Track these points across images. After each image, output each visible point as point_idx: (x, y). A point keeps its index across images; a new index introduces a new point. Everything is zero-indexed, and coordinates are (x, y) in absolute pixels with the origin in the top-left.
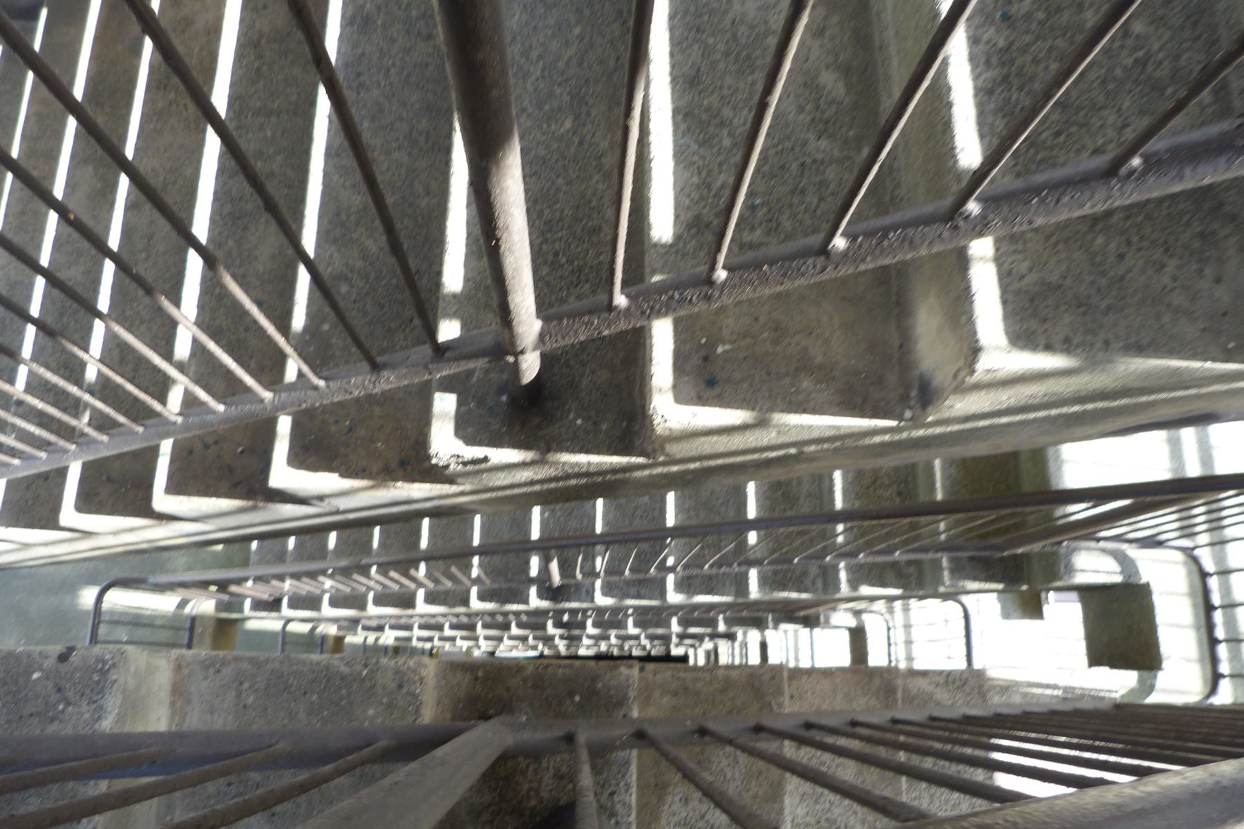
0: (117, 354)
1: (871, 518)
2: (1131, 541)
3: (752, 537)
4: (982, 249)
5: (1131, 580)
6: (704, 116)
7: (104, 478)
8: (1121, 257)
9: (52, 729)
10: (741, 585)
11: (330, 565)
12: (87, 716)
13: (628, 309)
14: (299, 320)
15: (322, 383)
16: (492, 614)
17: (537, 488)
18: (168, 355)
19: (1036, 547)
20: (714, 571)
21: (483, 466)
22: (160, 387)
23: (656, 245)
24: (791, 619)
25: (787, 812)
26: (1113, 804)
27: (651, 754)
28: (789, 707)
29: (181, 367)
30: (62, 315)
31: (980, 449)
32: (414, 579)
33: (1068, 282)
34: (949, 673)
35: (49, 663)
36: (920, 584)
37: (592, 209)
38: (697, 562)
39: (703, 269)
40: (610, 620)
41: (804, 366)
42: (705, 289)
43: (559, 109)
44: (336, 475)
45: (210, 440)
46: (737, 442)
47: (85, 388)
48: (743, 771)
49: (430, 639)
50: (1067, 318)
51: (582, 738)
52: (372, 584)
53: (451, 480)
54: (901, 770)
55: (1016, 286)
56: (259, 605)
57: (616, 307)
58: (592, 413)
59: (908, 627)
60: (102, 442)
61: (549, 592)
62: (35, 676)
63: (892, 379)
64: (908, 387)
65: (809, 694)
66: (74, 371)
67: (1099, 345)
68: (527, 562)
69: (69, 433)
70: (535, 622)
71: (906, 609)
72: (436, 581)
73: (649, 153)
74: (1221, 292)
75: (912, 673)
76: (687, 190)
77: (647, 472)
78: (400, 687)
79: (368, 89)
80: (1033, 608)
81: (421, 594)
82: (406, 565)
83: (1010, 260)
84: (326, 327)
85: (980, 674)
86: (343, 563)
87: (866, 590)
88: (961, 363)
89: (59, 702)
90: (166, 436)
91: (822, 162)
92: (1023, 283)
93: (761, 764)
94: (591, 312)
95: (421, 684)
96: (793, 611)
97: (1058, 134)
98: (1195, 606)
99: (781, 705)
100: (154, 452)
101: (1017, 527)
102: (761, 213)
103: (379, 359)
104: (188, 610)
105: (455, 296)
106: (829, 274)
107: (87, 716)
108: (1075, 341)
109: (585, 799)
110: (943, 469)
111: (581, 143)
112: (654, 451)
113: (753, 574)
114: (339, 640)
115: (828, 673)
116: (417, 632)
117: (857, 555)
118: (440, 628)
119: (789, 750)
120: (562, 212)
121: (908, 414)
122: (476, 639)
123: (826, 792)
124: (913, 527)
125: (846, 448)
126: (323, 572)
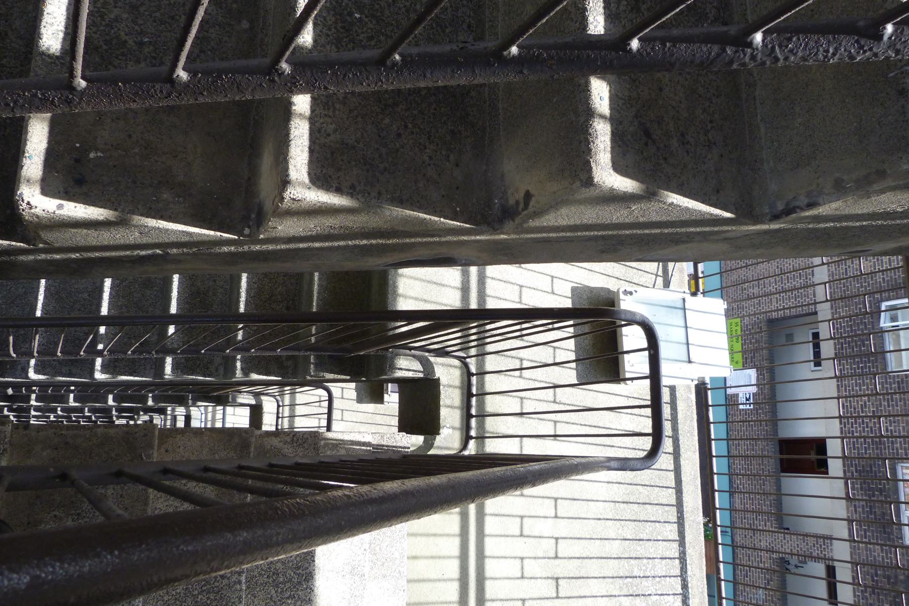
1: (258, 321)
2: (429, 351)
3: (171, 329)
8: (399, 135)
19: (372, 351)
20: (136, 356)
23: (43, 54)
33: (361, 145)
36: (294, 374)
46: (106, 237)
65: (182, 448)
67: (373, 194)
71: (293, 394)
77: (31, 257)
83: (322, 120)
87: (255, 377)
97: (370, 38)
98: (462, 394)
108: (358, 189)
113: (169, 360)
121: (247, 231)
125: (203, 254)
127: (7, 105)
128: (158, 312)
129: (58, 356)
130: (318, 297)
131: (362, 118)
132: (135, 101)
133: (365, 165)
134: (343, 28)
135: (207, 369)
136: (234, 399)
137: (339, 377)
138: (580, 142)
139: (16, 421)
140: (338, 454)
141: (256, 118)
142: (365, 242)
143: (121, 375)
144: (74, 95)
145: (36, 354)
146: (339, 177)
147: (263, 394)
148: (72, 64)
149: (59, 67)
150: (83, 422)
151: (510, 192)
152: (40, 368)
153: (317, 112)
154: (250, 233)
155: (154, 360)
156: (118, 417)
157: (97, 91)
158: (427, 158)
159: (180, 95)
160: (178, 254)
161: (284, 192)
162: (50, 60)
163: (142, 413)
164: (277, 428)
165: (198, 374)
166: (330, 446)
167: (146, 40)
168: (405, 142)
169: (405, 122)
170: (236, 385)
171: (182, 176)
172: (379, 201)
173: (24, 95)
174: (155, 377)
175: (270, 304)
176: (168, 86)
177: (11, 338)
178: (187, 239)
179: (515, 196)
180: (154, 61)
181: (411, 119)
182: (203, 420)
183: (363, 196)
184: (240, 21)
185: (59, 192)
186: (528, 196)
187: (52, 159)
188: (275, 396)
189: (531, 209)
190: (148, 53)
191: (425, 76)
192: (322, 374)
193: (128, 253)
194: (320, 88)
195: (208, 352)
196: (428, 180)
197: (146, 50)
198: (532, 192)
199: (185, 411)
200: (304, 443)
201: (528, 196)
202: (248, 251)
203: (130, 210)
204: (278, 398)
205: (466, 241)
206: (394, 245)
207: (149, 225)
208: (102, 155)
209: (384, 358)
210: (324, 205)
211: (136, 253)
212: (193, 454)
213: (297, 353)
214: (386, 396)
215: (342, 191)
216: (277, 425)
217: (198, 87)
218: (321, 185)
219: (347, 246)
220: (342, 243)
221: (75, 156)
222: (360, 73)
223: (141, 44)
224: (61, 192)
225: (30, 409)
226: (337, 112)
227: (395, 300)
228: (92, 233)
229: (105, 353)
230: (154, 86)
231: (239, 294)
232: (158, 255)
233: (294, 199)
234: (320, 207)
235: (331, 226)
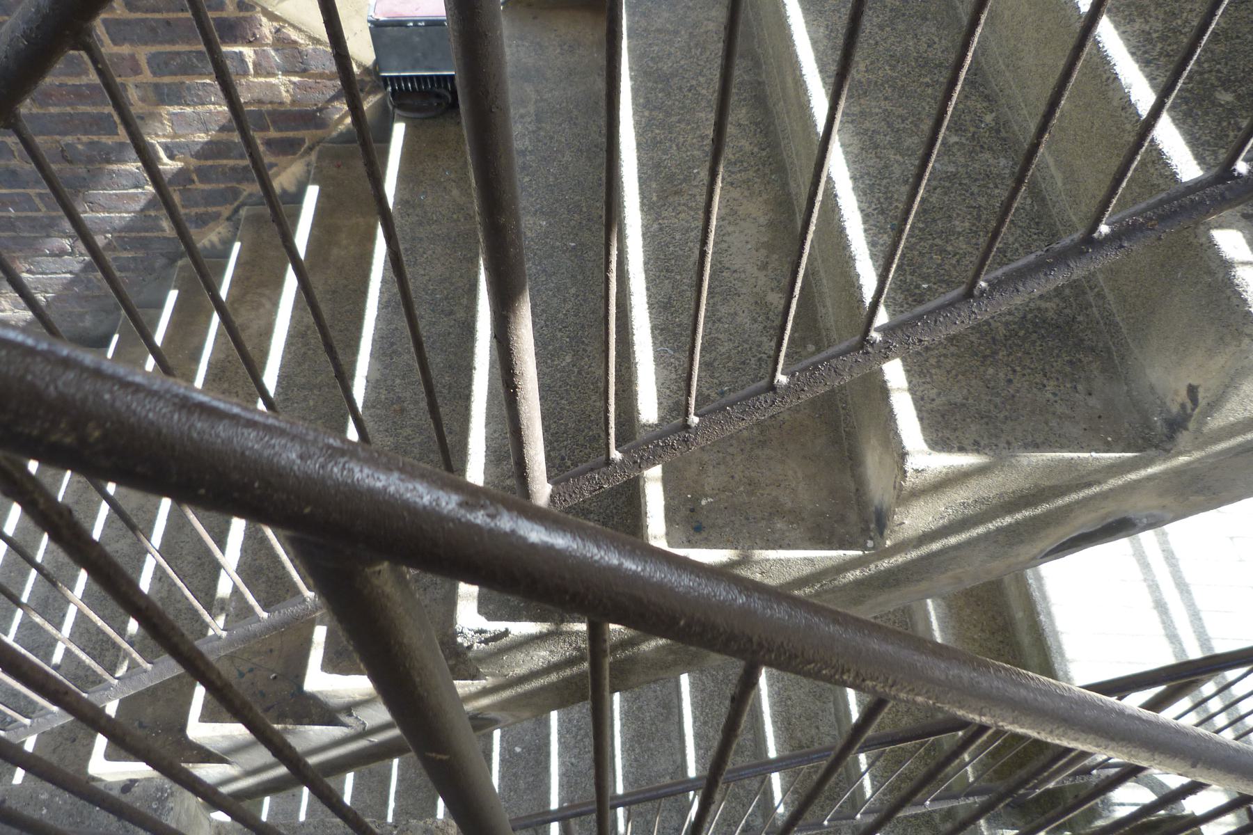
4: (894, 372)
6: (677, 330)
8: (1010, 381)
13: (622, 461)
21: (504, 641)
23: (645, 425)
33: (971, 401)
37: (592, 421)
41: (776, 511)
42: (683, 433)
43: (561, 348)
47: (126, 638)
55: (929, 406)
63: (853, 517)
64: (867, 522)
73: (634, 359)
74: (1092, 401)
79: (400, 355)
83: (921, 389)
94: (592, 470)
108: (982, 444)
111: (579, 373)
120: (567, 425)
121: (870, 544)
125: (826, 591)
127: (635, 462)
134: (915, 300)
138: (1229, 298)
142: (1008, 520)
151: (1168, 400)
158: (1050, 396)
168: (1019, 385)
176: (771, 393)
179: (1176, 399)
184: (805, 347)
186: (1192, 391)
189: (1202, 402)
191: (1018, 291)
194: (914, 344)
196: (1060, 418)
198: (1195, 383)
201: (1192, 391)
205: (1135, 481)
220: (981, 530)
234: (947, 474)
235: (964, 503)
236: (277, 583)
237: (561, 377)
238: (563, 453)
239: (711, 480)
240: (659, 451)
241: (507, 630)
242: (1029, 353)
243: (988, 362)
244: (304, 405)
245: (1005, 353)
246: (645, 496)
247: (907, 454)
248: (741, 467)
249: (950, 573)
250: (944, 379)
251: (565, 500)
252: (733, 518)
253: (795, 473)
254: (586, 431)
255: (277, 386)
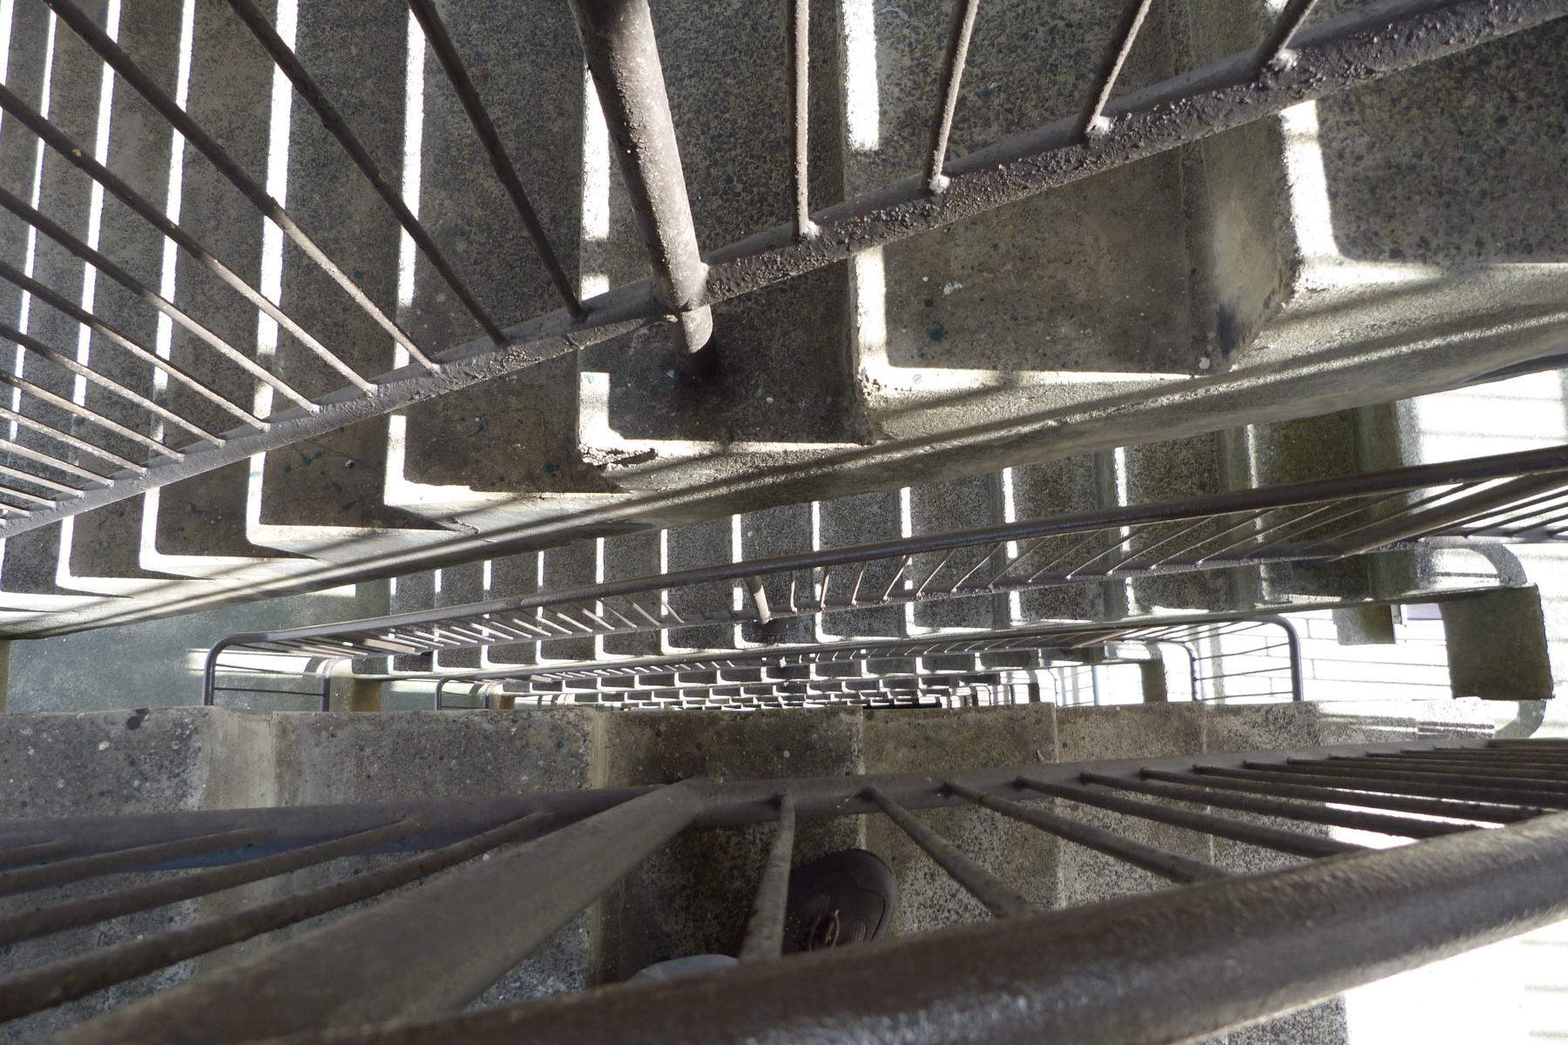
0: (190, 353)
4: (1301, 118)
5: (1512, 584)
7: (188, 508)
8: (1502, 121)
9: (129, 809)
10: (1000, 610)
11: (486, 607)
12: (168, 793)
13: (820, 239)
14: (406, 292)
15: (436, 367)
16: (691, 661)
17: (723, 490)
18: (250, 350)
19: (1384, 546)
20: (964, 595)
21: (649, 463)
22: (244, 390)
23: (857, 153)
24: (1067, 654)
25: (1060, 887)
26: (1489, 855)
27: (881, 819)
28: (1059, 756)
29: (266, 362)
30: (121, 308)
31: (1304, 407)
32: (589, 622)
33: (1426, 160)
34: (1269, 709)
35: (117, 731)
36: (1231, 601)
37: (775, 115)
38: (942, 585)
39: (918, 175)
40: (838, 663)
41: (1062, 305)
42: (921, 203)
44: (467, 488)
45: (310, 453)
46: (977, 413)
48: (1004, 838)
49: (619, 697)
50: (1423, 213)
51: (790, 801)
52: (539, 630)
53: (613, 489)
54: (1203, 826)
55: (1350, 170)
56: (405, 662)
57: (805, 236)
58: (786, 388)
59: (1217, 657)
60: (176, 462)
61: (758, 631)
62: (102, 746)
63: (1182, 317)
64: (1203, 327)
65: (1087, 739)
66: (139, 376)
68: (730, 595)
69: (139, 454)
70: (744, 669)
71: (1215, 636)
72: (617, 623)
73: (843, 28)
75: (1224, 711)
76: (897, 74)
77: (862, 462)
78: (559, 745)
80: (1380, 628)
81: (599, 640)
82: (579, 604)
83: (1342, 135)
84: (441, 298)
85: (1310, 708)
86: (500, 605)
87: (1159, 612)
88: (1276, 284)
89: (133, 777)
90: (255, 448)
91: (1080, 26)
92: (1360, 169)
93: (1026, 828)
94: (771, 247)
95: (585, 741)
96: (1069, 644)
99: (1049, 755)
100: (242, 469)
101: (1356, 520)
102: (996, 101)
103: (506, 331)
104: (320, 671)
105: (599, 243)
106: (1090, 169)
107: (168, 793)
108: (1434, 245)
109: (775, 870)
110: (1258, 437)
111: (754, 29)
112: (870, 433)
113: (1015, 597)
114: (507, 701)
115: (1111, 713)
116: (600, 688)
117: (1147, 568)
118: (629, 682)
119: (1061, 808)
121: (1204, 363)
122: (675, 694)
123: (1111, 860)
124: (1221, 525)
126: (478, 618)
127: (841, 242)
128: (985, 522)
129: (853, 606)
130: (1258, 459)
131: (1419, 108)
132: (1026, 187)
133: (1441, 194)
135: (1077, 605)
136: (1113, 653)
137: (1313, 599)
139: (786, 705)
140: (1350, 742)
141: (1188, 163)
142: (1437, 342)
143: (944, 626)
144: (932, 203)
145: (823, 605)
146: (1393, 231)
147: (1162, 640)
148: (933, 154)
149: (880, 168)
150: (875, 701)
152: (830, 625)
153: (1329, 122)
154: (1211, 366)
155: (990, 599)
156: (925, 693)
157: (967, 187)
159: (1099, 157)
160: (1082, 423)
161: (1294, 281)
162: (868, 161)
163: (962, 684)
164: (1194, 699)
165: (1063, 615)
166: (1333, 728)
167: (993, 85)
168: (1517, 129)
169: (1509, 91)
170: (1117, 628)
171: (1084, 292)
172: (1481, 258)
173: (862, 221)
174: (995, 624)
175: (1169, 483)
177: (793, 585)
178: (1102, 394)
180: (1010, 116)
181: (1521, 81)
182: (1059, 690)
183: (1446, 256)
185: (912, 357)
187: (895, 309)
188: (1183, 642)
190: (999, 105)
192: (1286, 596)
193: (1003, 433)
195: (1077, 578)
197: (996, 102)
199: (1028, 677)
200: (1288, 724)
202: (1204, 398)
203: (1015, 364)
204: (1189, 645)
206: (1499, 337)
207: (1047, 383)
208: (961, 286)
209: (1409, 556)
210: (1368, 290)
211: (1014, 431)
212: (1106, 749)
213: (1234, 564)
214: (1397, 627)
215: (1404, 256)
216: (1194, 693)
217: (1130, 137)
218: (1361, 252)
219: (1399, 356)
220: (1388, 353)
221: (924, 297)
222: (1443, 23)
223: (987, 95)
224: (915, 356)
225: (805, 686)
226: (1368, 111)
227: (1415, 442)
228: (958, 410)
229: (919, 594)
230: (1055, 155)
231: (1113, 472)
232: (1053, 429)
233: (1314, 291)
234: (1361, 294)
236: (337, 333)
237: (725, 36)
238: (729, 168)
239: (961, 252)
240: (881, 228)
241: (652, 450)
242: (1546, 64)
243: (1470, 82)
244: (343, 53)
245: (1502, 62)
246: (855, 278)
247: (1301, 262)
248: (1009, 229)
249: (1318, 397)
250: (1385, 116)
251: (729, 290)
252: (992, 318)
253: (1096, 239)
254: (766, 132)
255: (299, 22)
